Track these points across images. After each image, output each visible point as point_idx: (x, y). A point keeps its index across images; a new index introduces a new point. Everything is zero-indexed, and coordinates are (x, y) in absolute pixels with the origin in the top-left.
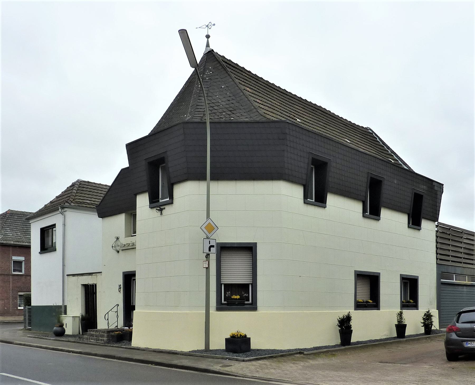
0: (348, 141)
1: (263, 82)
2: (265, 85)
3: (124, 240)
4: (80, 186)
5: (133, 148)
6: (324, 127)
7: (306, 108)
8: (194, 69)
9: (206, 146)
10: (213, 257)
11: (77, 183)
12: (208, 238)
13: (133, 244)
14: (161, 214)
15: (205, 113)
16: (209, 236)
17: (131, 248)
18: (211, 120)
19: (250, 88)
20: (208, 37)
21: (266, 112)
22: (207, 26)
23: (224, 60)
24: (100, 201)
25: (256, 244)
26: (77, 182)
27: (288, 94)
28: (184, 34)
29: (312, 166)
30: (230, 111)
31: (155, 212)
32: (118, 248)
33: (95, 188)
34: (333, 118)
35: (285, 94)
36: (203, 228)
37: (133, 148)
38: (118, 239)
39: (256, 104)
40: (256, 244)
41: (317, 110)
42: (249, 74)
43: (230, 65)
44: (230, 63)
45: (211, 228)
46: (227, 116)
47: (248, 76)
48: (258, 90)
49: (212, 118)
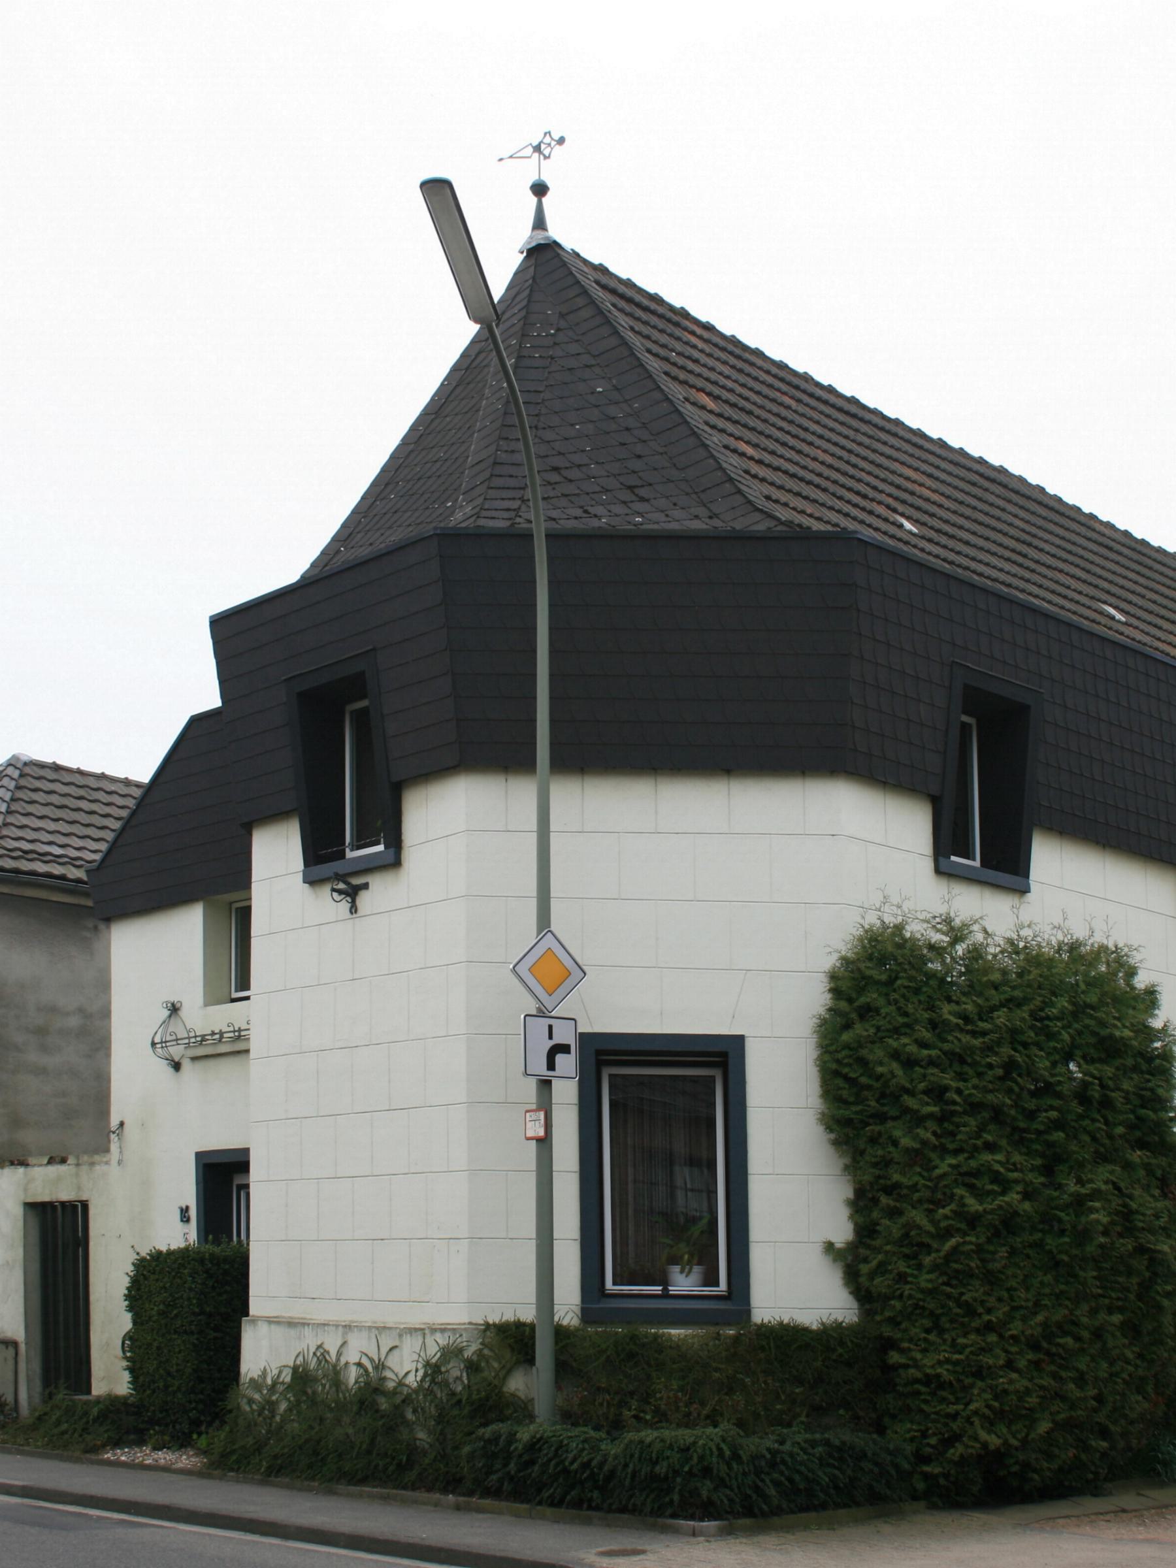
0: (1118, 616)
1: (766, 366)
2: (770, 380)
3: (202, 1017)
4: (23, 782)
5: (234, 632)
6: (1014, 557)
7: (943, 476)
8: (478, 327)
9: (553, 722)
10: (566, 1092)
11: (10, 771)
12: (542, 1013)
13: (239, 1036)
14: (354, 909)
15: (528, 494)
16: (549, 1002)
17: (230, 1047)
18: (553, 525)
19: (709, 394)
20: (540, 189)
21: (776, 494)
22: (537, 149)
23: (604, 280)
24: (103, 846)
25: (739, 1041)
26: (10, 764)
27: (868, 416)
28: (439, 194)
29: (965, 718)
30: (631, 488)
31: (326, 905)
32: (176, 1051)
33: (81, 792)
34: (1057, 518)
35: (854, 416)
36: (523, 969)
37: (234, 632)
38: (174, 1009)
39: (734, 460)
40: (739, 1041)
41: (986, 484)
42: (706, 335)
43: (630, 300)
44: (629, 293)
45: (552, 972)
46: (619, 509)
47: (700, 344)
48: (742, 403)
49: (554, 514)
